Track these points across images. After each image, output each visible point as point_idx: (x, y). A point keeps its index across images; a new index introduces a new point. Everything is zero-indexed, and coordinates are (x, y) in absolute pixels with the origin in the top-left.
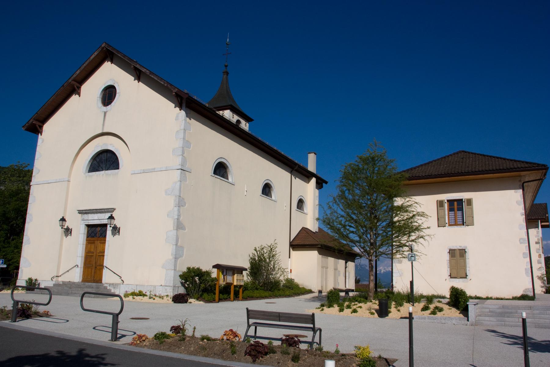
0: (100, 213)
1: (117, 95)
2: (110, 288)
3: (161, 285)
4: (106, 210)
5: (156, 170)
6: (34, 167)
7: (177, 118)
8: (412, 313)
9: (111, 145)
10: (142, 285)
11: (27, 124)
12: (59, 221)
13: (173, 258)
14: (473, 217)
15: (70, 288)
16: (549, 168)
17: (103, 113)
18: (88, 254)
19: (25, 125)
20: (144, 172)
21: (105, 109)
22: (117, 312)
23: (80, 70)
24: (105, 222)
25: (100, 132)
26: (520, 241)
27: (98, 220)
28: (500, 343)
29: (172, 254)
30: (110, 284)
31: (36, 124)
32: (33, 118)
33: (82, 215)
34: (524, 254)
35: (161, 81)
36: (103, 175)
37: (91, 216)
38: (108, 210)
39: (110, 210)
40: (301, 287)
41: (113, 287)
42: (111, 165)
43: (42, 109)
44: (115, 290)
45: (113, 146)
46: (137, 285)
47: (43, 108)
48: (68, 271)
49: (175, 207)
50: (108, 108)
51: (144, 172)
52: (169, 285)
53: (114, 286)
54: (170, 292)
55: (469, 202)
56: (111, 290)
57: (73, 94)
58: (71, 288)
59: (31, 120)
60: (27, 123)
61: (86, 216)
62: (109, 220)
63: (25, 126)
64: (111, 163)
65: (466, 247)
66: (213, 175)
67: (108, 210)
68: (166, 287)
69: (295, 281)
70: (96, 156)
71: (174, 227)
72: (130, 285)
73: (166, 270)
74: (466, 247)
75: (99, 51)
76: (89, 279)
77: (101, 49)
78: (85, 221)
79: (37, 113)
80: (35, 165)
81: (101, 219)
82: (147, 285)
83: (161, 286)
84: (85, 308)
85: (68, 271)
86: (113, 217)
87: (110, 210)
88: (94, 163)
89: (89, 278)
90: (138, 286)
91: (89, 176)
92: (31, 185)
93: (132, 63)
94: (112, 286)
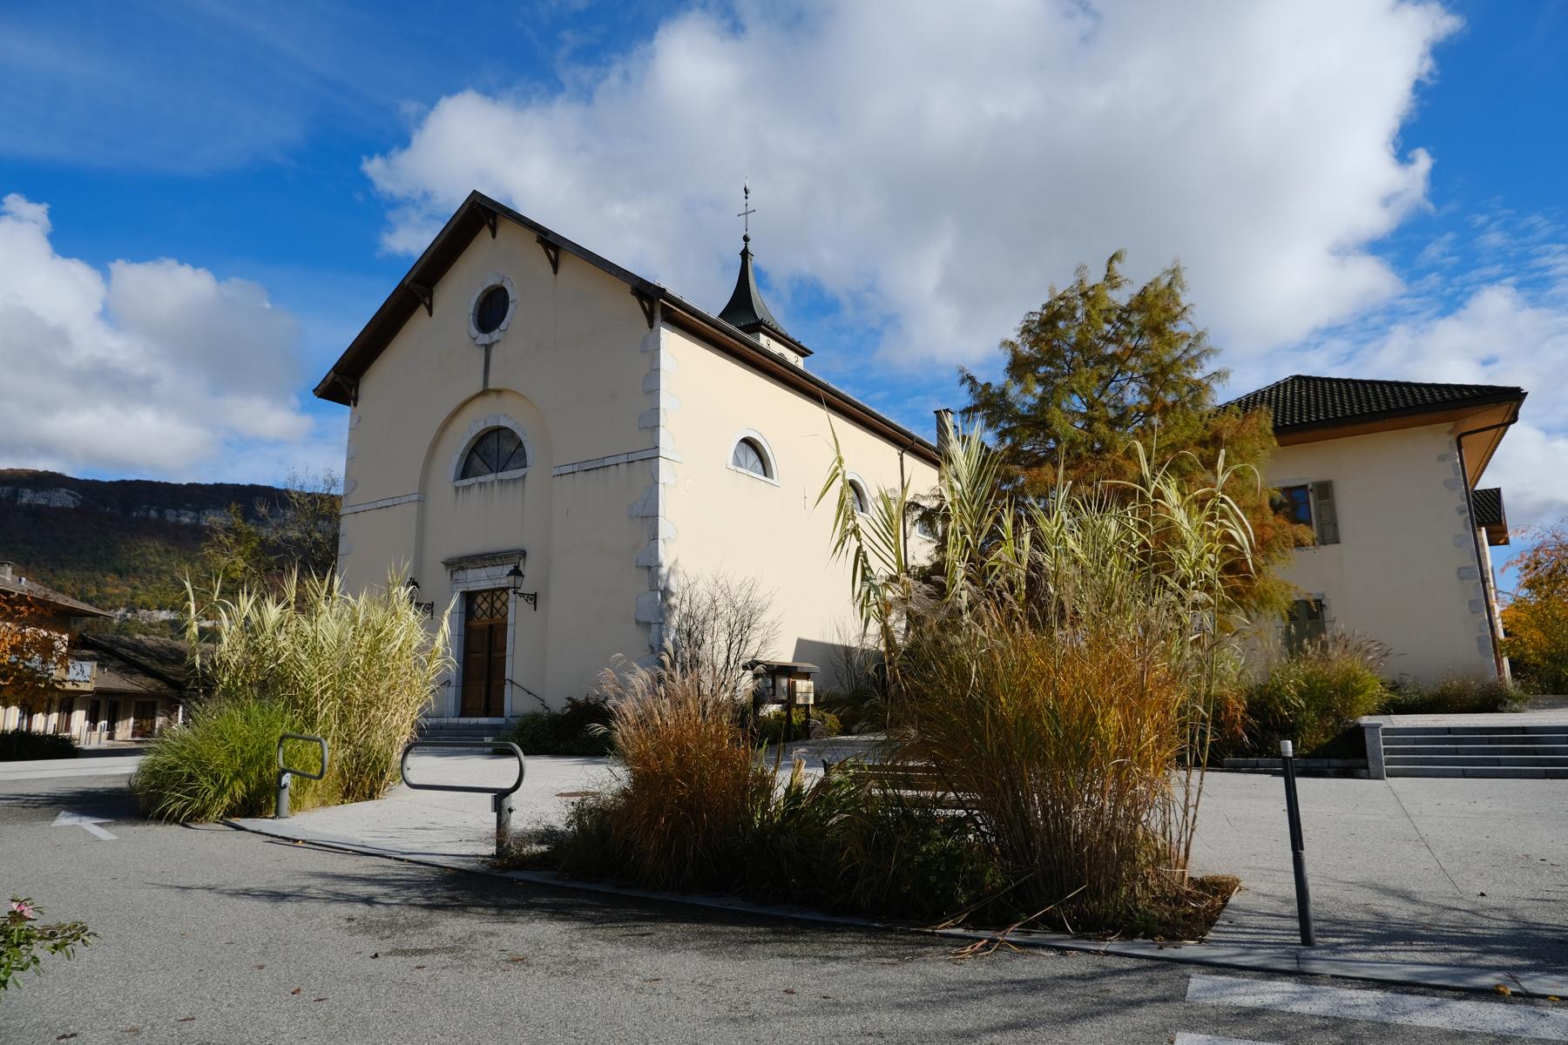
1: (511, 306)
9: (505, 415)
14: (1335, 525)
16: (1528, 397)
21: (485, 338)
22: (510, 784)
24: (504, 583)
26: (1459, 573)
34: (1471, 603)
40: (76, 259)
45: (511, 418)
48: (529, 693)
55: (1325, 490)
62: (512, 578)
65: (1323, 595)
66: (733, 467)
69: (668, 291)
74: (1323, 595)
81: (497, 576)
84: (414, 781)
85: (529, 693)
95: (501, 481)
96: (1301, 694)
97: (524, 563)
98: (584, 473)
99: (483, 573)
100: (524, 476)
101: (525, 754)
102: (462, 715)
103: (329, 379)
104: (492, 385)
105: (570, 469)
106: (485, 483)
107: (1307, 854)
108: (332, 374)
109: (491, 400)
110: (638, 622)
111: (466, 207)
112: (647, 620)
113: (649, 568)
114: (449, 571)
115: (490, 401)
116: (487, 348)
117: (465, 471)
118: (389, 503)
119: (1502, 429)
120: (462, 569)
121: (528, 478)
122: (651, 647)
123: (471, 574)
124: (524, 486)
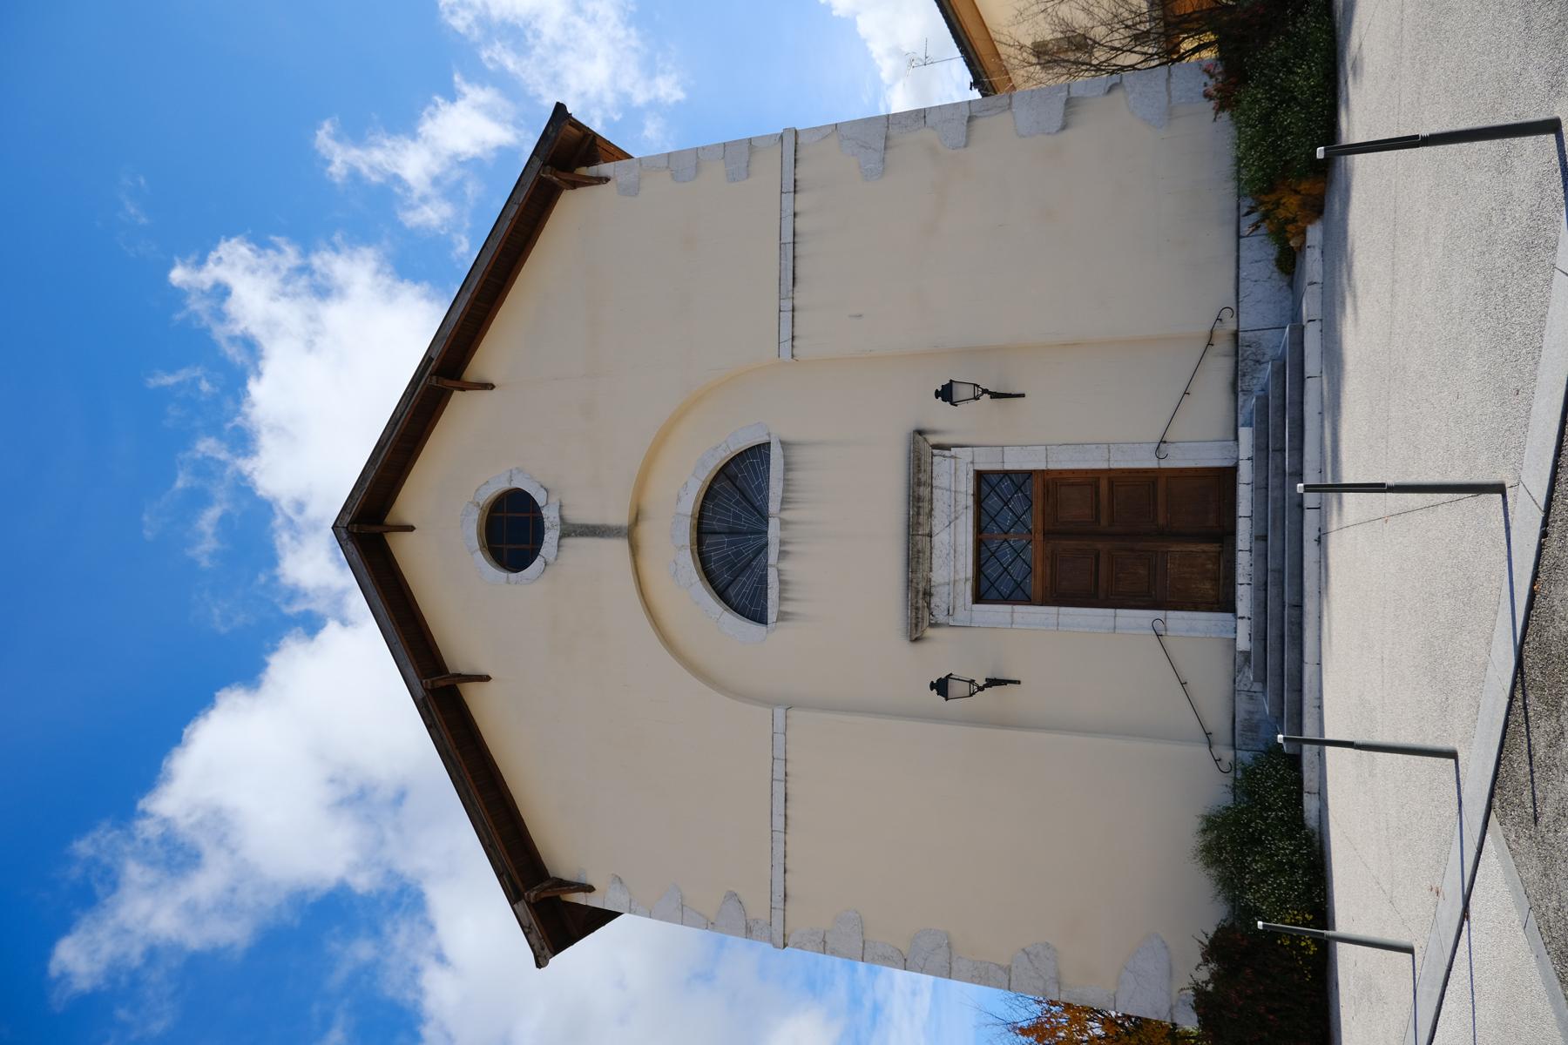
50: (551, 519)
57: (1336, 945)
95: (784, 501)
96: (1215, 90)
97: (934, 432)
98: (798, 286)
99: (942, 539)
100: (784, 445)
101: (1335, 143)
102: (1228, 606)
103: (530, 918)
104: (620, 518)
105: (787, 316)
106: (782, 543)
107: (1390, 481)
108: (521, 906)
109: (646, 531)
110: (1064, 127)
111: (351, 547)
112: (1060, 106)
113: (970, 119)
114: (930, 632)
115: (649, 533)
116: (570, 531)
117: (752, 607)
118: (779, 788)
119: (982, 510)
120: (928, 594)
121: (789, 436)
122: (1111, 89)
123: (940, 574)
124: (799, 444)
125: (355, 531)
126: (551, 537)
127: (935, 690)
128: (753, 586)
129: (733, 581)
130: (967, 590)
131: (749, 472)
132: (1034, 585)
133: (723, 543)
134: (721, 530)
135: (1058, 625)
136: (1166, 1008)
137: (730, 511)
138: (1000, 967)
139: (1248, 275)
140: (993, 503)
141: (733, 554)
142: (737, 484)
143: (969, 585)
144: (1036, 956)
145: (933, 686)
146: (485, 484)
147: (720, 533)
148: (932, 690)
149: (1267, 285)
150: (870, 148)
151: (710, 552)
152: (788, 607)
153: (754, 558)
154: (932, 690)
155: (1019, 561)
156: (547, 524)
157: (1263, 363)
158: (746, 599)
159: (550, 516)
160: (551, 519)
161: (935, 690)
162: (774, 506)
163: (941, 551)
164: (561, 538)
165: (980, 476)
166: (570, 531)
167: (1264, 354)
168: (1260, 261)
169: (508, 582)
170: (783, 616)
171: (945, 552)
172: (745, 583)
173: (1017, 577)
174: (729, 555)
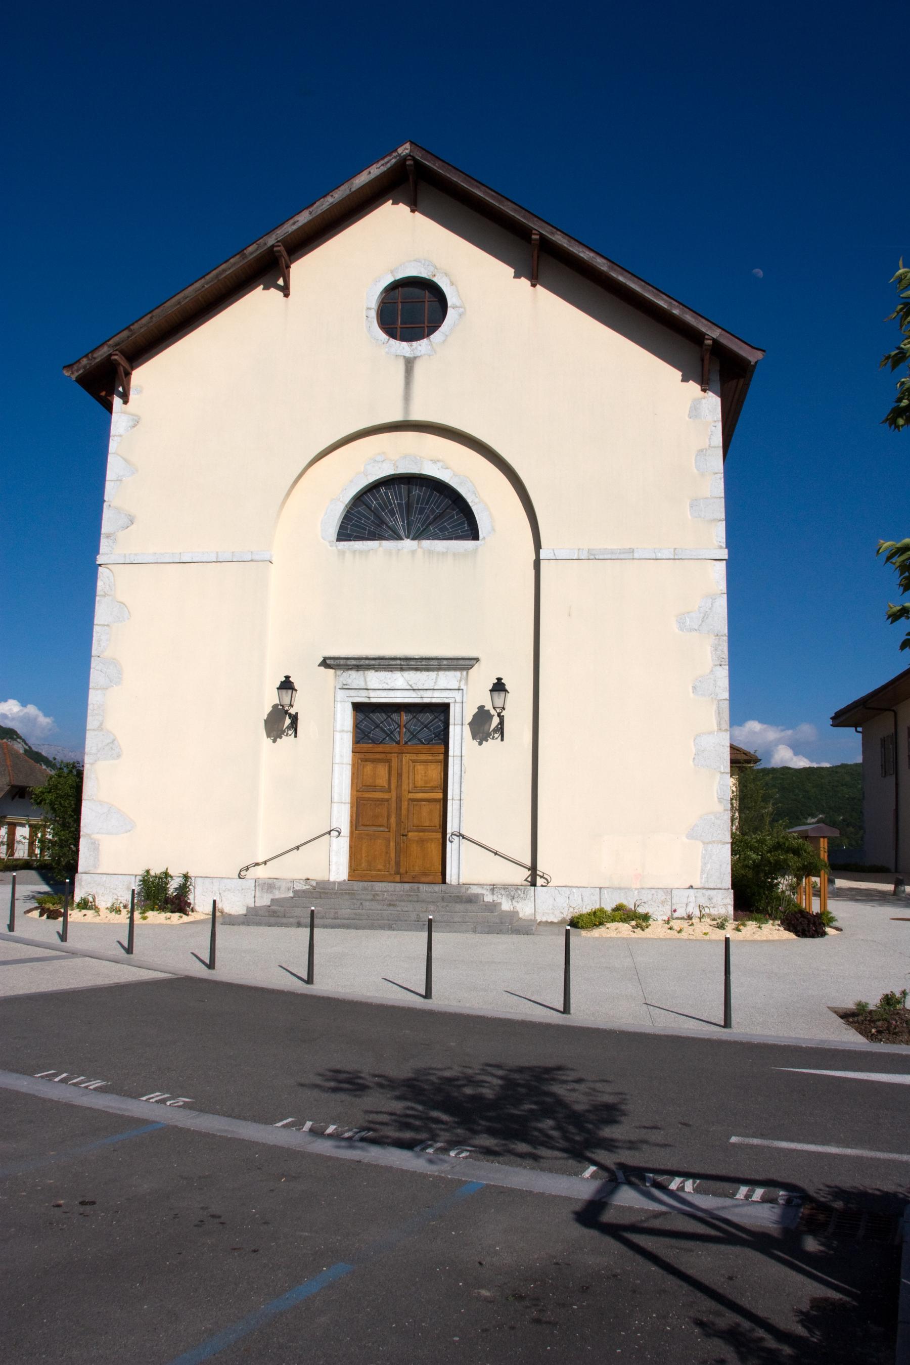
0: (416, 669)
2: (495, 898)
3: (691, 887)
4: (445, 662)
5: (636, 555)
6: (105, 505)
7: (695, 412)
8: (729, 938)
10: (620, 888)
11: (85, 361)
12: (278, 689)
13: (725, 810)
15: (390, 905)
17: (401, 367)
18: (367, 795)
19: (79, 361)
20: (593, 556)
23: (310, 213)
25: (397, 416)
27: (412, 691)
28: (504, 993)
29: (720, 800)
30: (493, 888)
31: (119, 364)
32: (111, 342)
33: (339, 672)
35: (656, 298)
36: (413, 552)
37: (375, 679)
38: (455, 662)
39: (461, 662)
41: (507, 896)
42: (430, 524)
43: (151, 318)
44: (515, 904)
46: (601, 888)
47: (154, 313)
49: (718, 667)
50: (419, 348)
51: (593, 556)
52: (719, 886)
53: (512, 893)
54: (725, 905)
56: (501, 904)
57: (259, 285)
58: (394, 905)
59: (104, 351)
60: (86, 356)
61: (355, 678)
63: (75, 367)
64: (428, 517)
67: (455, 662)
68: (710, 892)
70: (366, 489)
71: (719, 724)
72: (574, 890)
73: (704, 843)
75: (389, 165)
76: (379, 870)
77: (394, 161)
78: (352, 693)
79: (128, 328)
80: (106, 498)
82: (638, 886)
83: (691, 890)
85: (298, 848)
86: (290, 682)
87: (461, 662)
88: (359, 512)
89: (380, 867)
90: (605, 891)
91: (354, 552)
92: (98, 563)
93: (534, 224)
94: (503, 892)
100: (475, 551)
116: (409, 364)
125: (407, 163)
126: (404, 348)
127: (496, 681)
128: (367, 526)
129: (371, 509)
130: (361, 698)
131: (457, 520)
132: (434, 772)
133: (401, 500)
134: (411, 498)
135: (343, 764)
136: (89, 832)
137: (427, 504)
138: (101, 724)
139: (573, 893)
140: (427, 717)
141: (392, 509)
142: (448, 510)
143: (365, 700)
144: (112, 748)
145: (499, 679)
146: (451, 282)
147: (409, 497)
148: (497, 679)
149: (565, 905)
150: (702, 621)
151: (394, 488)
152: (348, 556)
153: (389, 527)
154: (497, 679)
155: (384, 736)
156: (414, 344)
157: (512, 902)
158: (356, 521)
159: (421, 346)
160: (419, 348)
161: (496, 681)
162: (426, 543)
163: (390, 679)
164: (404, 357)
165: (444, 708)
166: (409, 364)
167: (518, 902)
168: (582, 901)
169: (369, 309)
170: (342, 553)
171: (389, 681)
172: (369, 519)
173: (373, 734)
174: (365, 529)
